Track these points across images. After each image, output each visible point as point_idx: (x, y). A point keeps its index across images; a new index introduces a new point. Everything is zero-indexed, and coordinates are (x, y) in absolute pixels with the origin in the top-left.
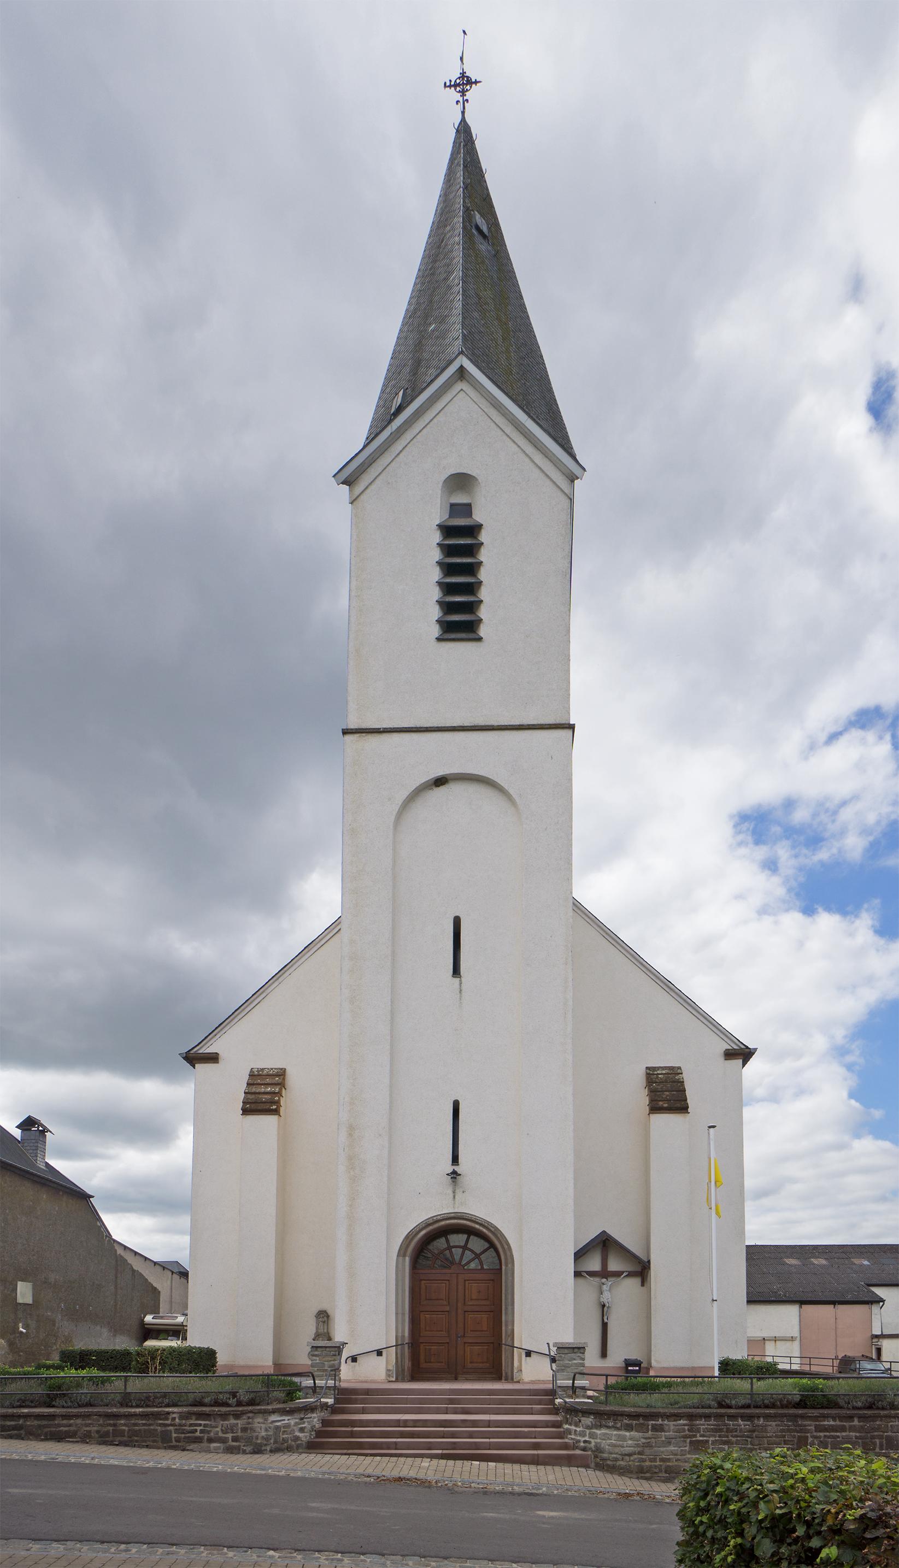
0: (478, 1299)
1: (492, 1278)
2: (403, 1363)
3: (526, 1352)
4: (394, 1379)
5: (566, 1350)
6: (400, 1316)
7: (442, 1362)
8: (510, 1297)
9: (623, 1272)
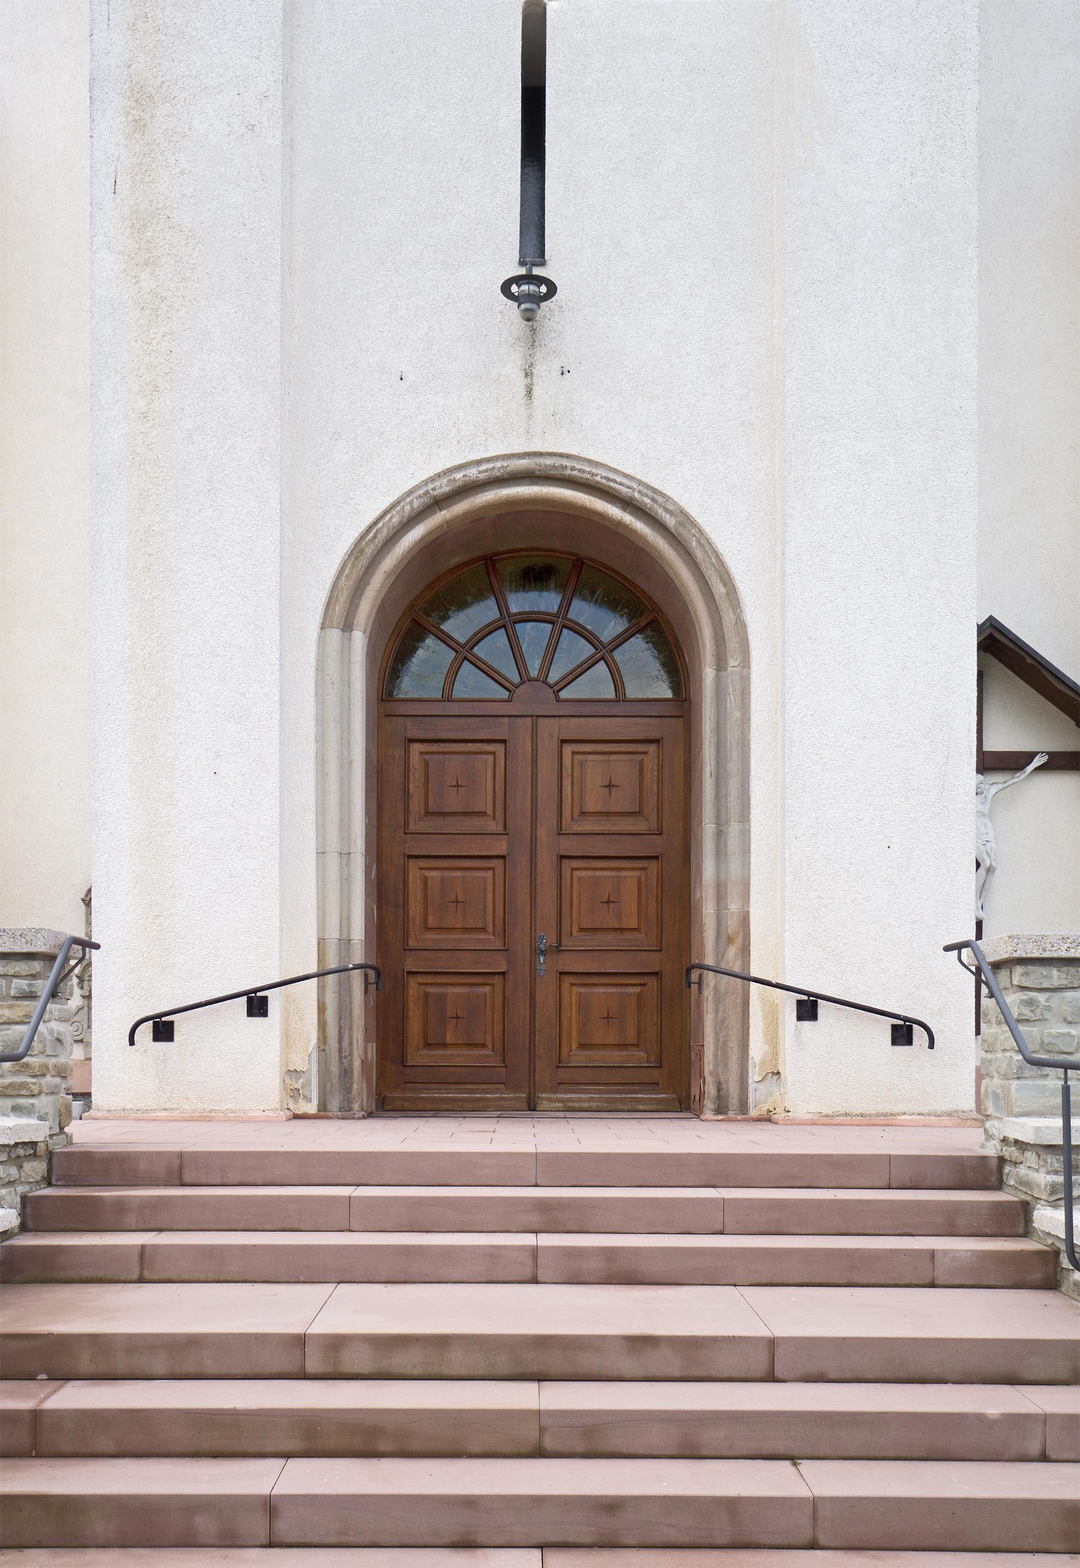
0: (607, 814)
1: (655, 735)
2: (345, 1044)
3: (800, 1003)
4: (312, 1108)
5: (1055, 972)
6: (333, 862)
7: (484, 1045)
8: (733, 786)
9: (1031, 756)
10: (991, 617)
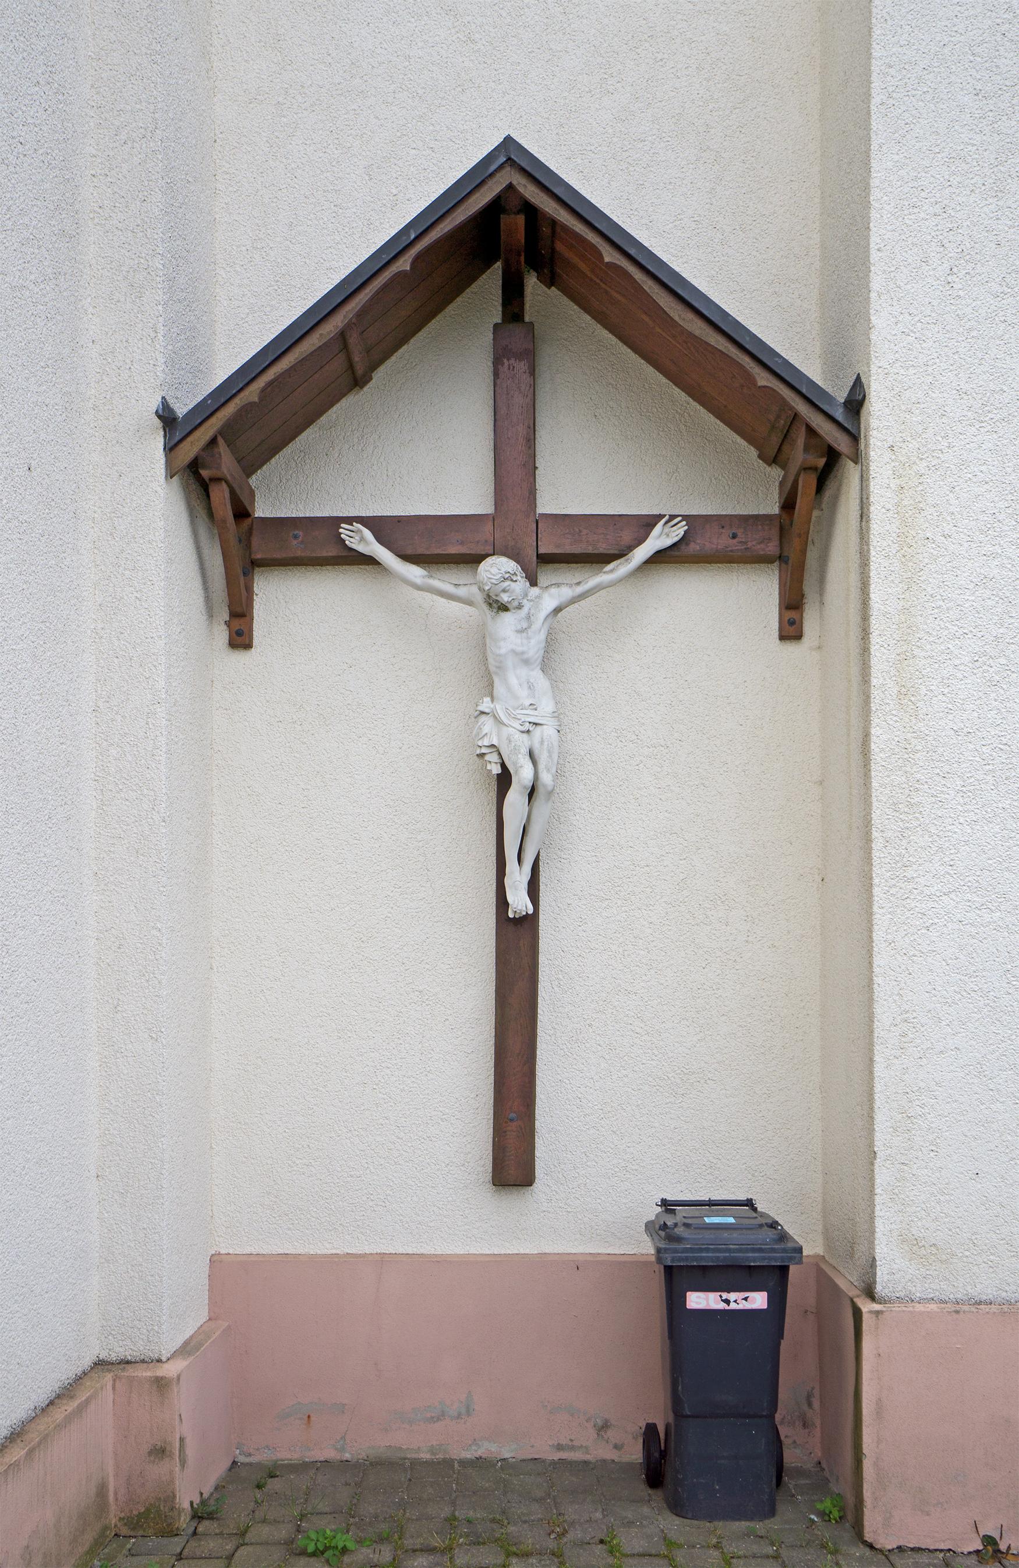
9: (647, 524)
10: (508, 139)
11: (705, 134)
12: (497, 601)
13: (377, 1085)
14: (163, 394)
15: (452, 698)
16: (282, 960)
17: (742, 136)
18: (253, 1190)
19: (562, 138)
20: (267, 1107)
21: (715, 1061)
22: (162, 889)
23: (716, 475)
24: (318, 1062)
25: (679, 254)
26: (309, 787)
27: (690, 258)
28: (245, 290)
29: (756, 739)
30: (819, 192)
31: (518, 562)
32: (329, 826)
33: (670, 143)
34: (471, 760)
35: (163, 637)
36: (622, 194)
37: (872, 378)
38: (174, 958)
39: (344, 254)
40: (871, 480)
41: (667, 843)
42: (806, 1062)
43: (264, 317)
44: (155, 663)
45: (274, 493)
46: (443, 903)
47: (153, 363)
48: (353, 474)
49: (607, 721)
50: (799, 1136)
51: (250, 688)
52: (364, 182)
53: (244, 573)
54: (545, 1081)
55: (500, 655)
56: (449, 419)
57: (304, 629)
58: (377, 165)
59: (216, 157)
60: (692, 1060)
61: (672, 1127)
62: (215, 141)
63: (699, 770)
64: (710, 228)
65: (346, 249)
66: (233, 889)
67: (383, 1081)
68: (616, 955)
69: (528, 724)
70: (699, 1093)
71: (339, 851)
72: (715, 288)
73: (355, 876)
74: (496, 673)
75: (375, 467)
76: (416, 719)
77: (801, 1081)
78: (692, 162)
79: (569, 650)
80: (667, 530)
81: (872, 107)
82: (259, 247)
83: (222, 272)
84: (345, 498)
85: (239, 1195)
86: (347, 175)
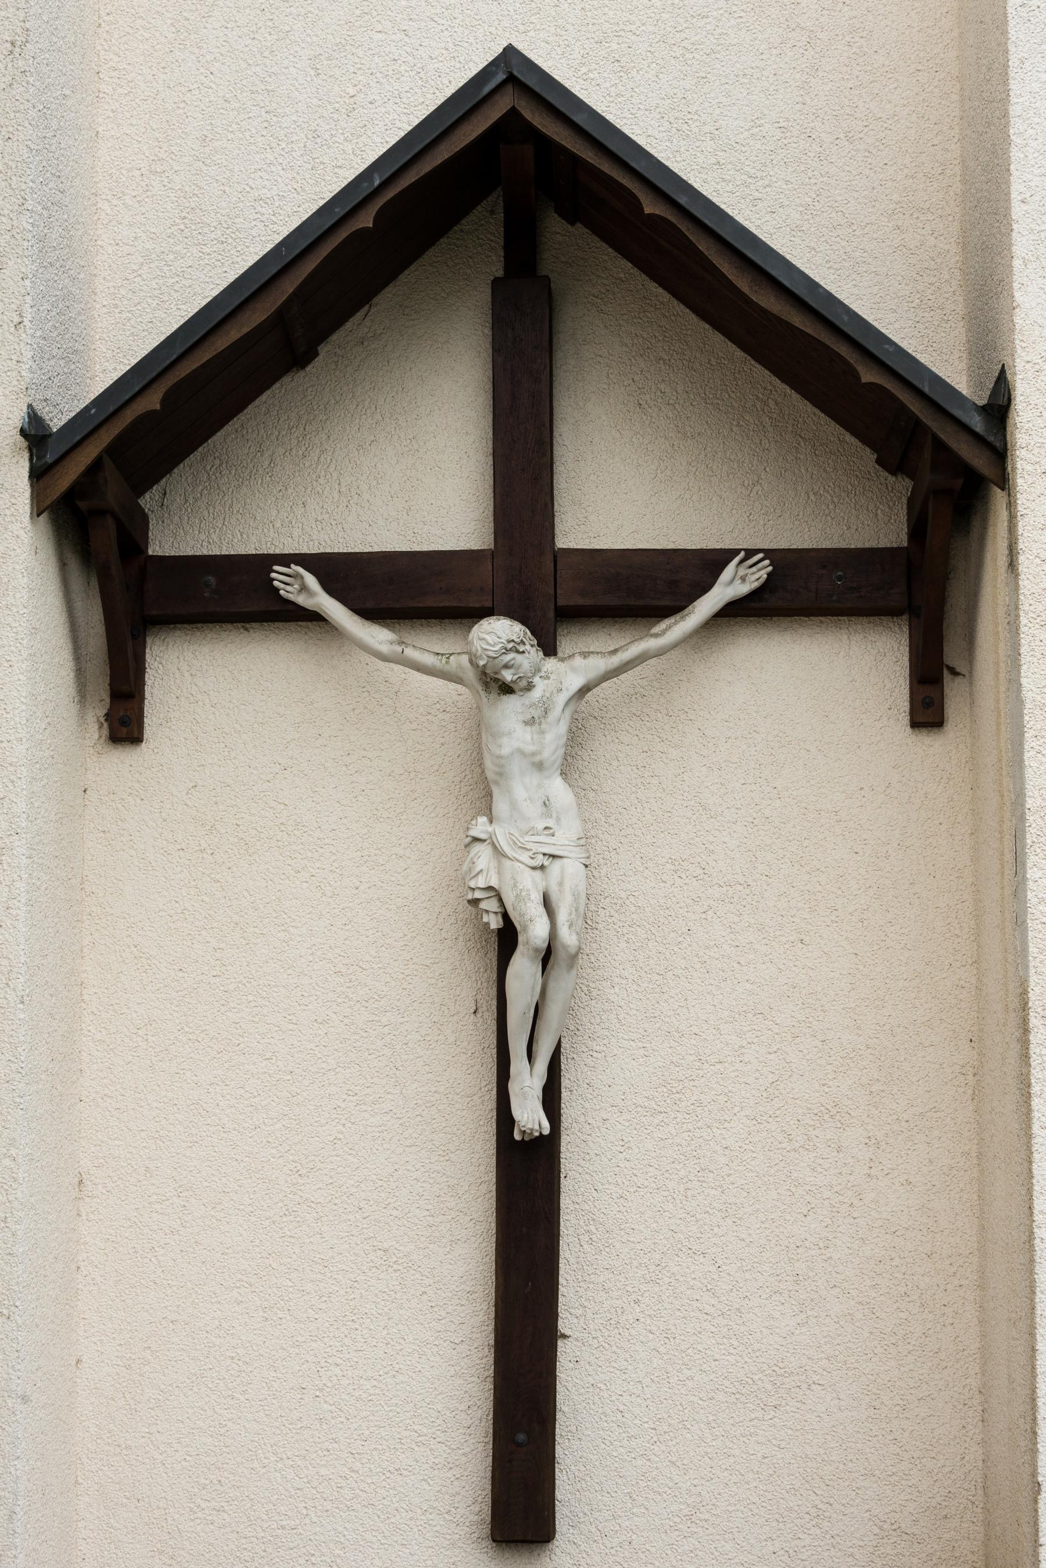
10: (510, 52)
11: (793, 6)
12: (496, 680)
13: (321, 1390)
14: (29, 400)
15: (433, 815)
16: (182, 1203)
17: (846, 8)
18: (138, 1546)
19: (589, 14)
20: (158, 1422)
21: (823, 1355)
22: (18, 1100)
23: (816, 488)
24: (233, 1355)
25: (759, 174)
26: (223, 945)
27: (774, 179)
28: (138, 231)
29: (879, 873)
30: (958, 87)
31: (523, 622)
32: (253, 1004)
33: (744, 20)
34: (460, 906)
35: (24, 740)
36: (675, 91)
37: (1018, 376)
38: (32, 1200)
39: (279, 179)
40: (1019, 518)
41: (749, 1028)
42: (958, 1357)
43: (166, 268)
44: (12, 777)
45: (176, 518)
46: (419, 1118)
47: (17, 359)
48: (290, 491)
49: (659, 847)
50: (947, 1469)
51: (139, 801)
52: (309, 79)
53: (133, 635)
54: (570, 1386)
55: (500, 757)
56: (428, 410)
57: (217, 714)
58: (327, 55)
59: (99, 48)
60: (789, 1355)
61: (759, 1455)
62: (100, 25)
63: (795, 919)
64: (802, 137)
65: (282, 173)
66: (111, 1097)
67: (329, 1385)
68: (675, 1196)
69: (542, 856)
70: (799, 1405)
71: (267, 1040)
72: (811, 221)
73: (289, 1077)
74: (497, 783)
75: (322, 481)
76: (381, 845)
77: (951, 1385)
78: (776, 45)
79: (603, 744)
80: (742, 571)
81: (1010, 10)
82: (158, 170)
83: (106, 206)
84: (278, 525)
85: (117, 1554)
86: (284, 70)
